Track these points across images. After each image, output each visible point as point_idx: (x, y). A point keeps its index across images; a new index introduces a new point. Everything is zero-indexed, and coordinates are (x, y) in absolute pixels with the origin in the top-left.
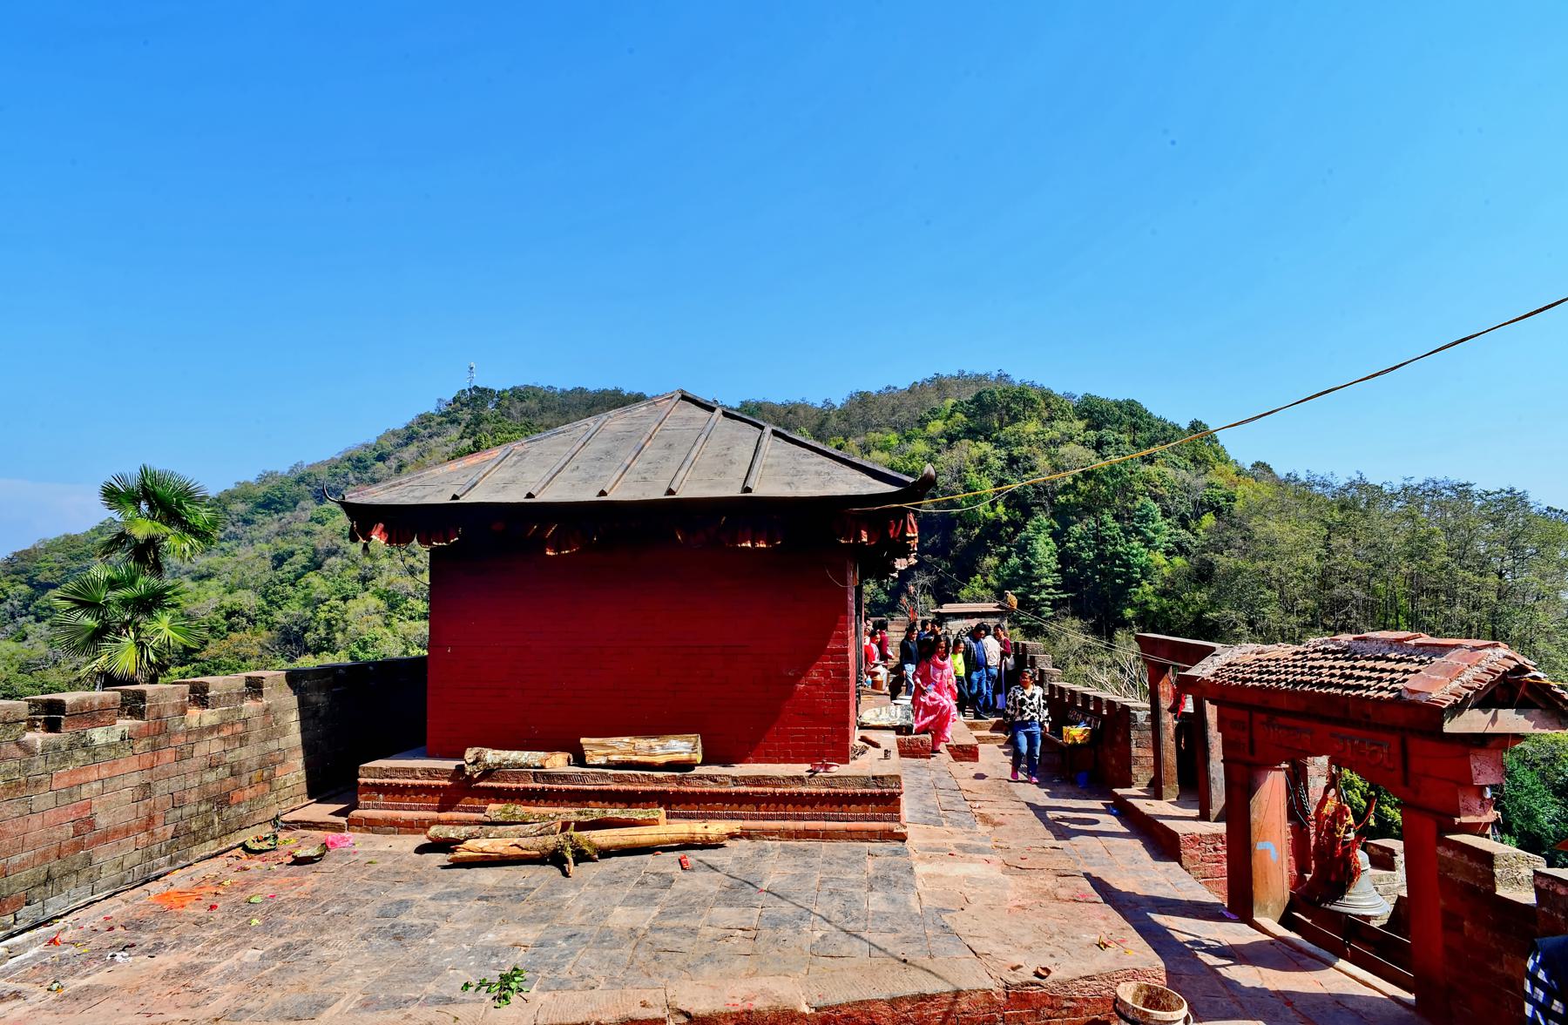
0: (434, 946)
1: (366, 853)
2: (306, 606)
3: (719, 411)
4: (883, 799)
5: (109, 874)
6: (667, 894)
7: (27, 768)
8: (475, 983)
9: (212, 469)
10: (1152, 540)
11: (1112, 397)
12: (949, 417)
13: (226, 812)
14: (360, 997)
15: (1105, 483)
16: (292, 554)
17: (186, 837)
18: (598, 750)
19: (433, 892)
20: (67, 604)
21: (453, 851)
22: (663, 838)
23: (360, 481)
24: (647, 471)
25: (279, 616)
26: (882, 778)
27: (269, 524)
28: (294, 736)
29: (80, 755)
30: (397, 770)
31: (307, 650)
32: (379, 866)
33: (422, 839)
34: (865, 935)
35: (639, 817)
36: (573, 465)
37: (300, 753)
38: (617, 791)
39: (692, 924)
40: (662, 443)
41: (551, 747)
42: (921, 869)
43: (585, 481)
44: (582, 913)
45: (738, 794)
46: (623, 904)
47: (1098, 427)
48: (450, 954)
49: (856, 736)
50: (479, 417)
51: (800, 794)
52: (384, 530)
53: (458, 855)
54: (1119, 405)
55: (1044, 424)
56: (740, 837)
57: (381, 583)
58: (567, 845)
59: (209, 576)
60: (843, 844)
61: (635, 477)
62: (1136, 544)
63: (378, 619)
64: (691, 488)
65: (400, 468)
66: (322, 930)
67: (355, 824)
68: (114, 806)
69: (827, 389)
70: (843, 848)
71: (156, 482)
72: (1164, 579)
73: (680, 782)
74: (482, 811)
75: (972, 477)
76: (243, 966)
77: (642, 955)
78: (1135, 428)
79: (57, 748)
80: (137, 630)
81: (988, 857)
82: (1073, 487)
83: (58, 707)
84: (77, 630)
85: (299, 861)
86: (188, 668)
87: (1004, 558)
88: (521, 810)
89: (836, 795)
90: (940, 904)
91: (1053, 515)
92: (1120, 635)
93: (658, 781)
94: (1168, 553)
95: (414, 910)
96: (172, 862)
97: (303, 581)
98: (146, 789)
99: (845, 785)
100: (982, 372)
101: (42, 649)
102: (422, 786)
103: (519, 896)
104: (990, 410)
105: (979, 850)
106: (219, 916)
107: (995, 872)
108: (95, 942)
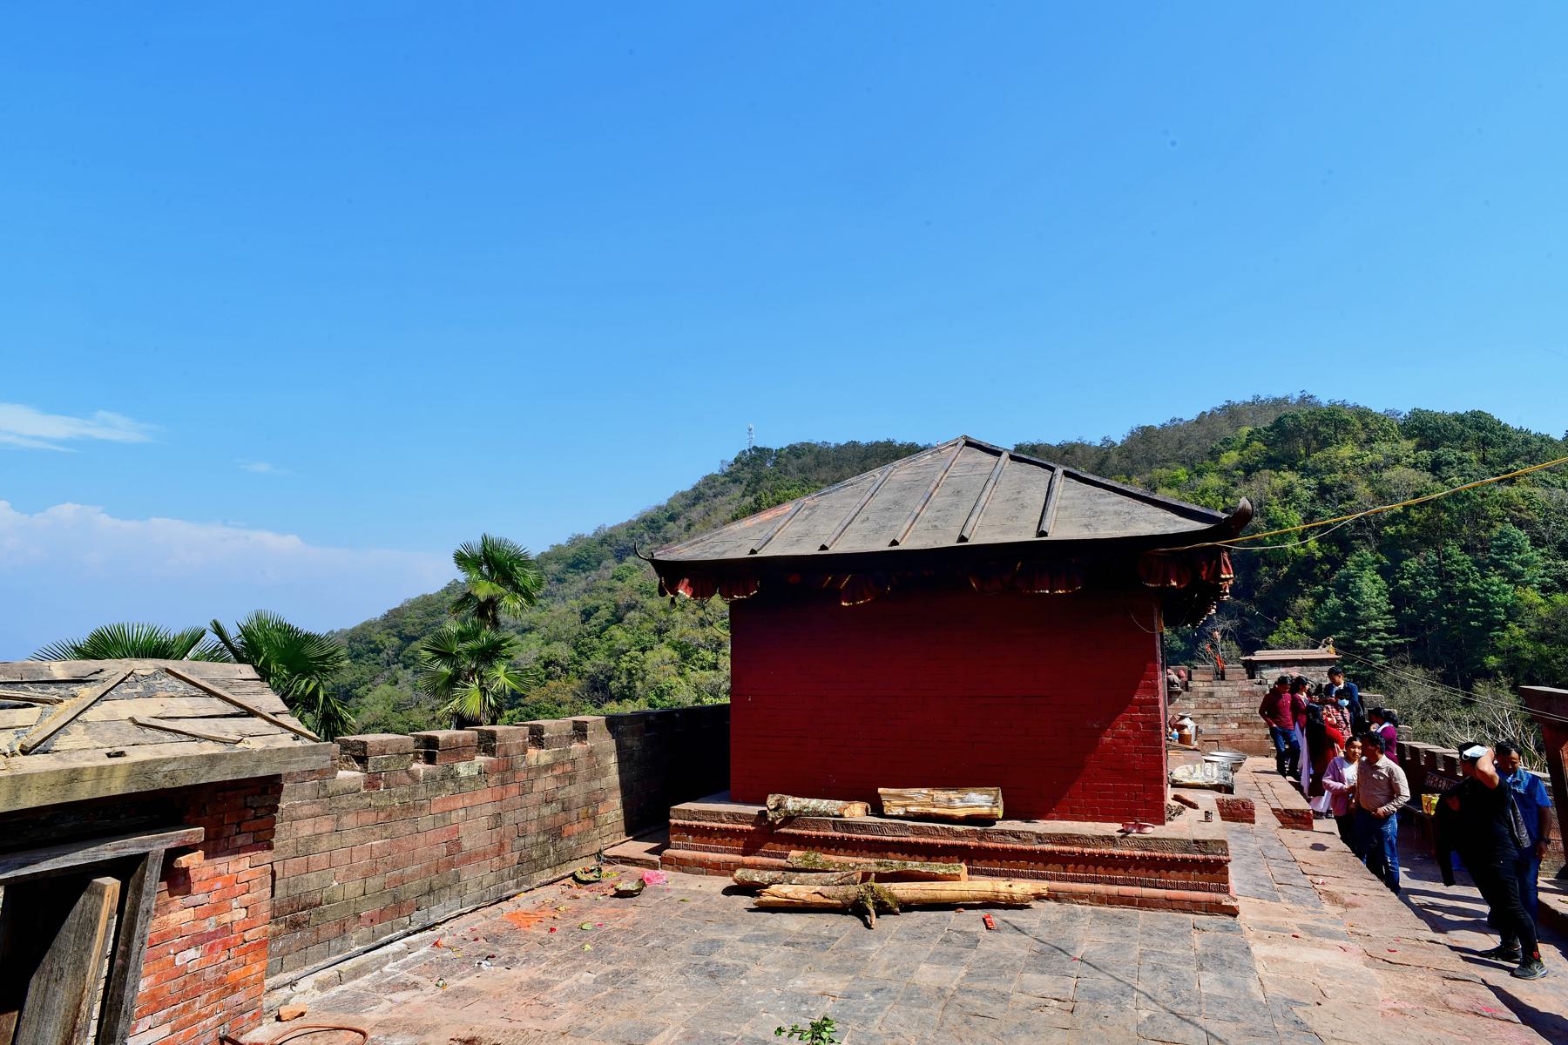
0: (746, 987)
1: (678, 892)
2: (610, 656)
3: (1005, 455)
4: (1207, 867)
5: (473, 892)
6: (972, 956)
7: (414, 794)
8: (788, 1029)
9: (534, 536)
10: (1521, 574)
11: (1449, 410)
12: (1245, 447)
13: (559, 844)
14: (682, 1030)
15: (1446, 510)
16: (597, 609)
17: (528, 865)
18: (904, 801)
19: (739, 929)
20: (429, 655)
21: (759, 895)
22: (966, 894)
23: (654, 540)
24: (937, 518)
25: (587, 666)
26: (1205, 842)
27: (578, 582)
28: (613, 777)
29: (450, 785)
30: (704, 813)
31: (611, 697)
32: (691, 904)
33: (729, 881)
34: (1199, 1020)
35: (940, 871)
36: (863, 516)
37: (618, 793)
38: (917, 844)
39: (1003, 988)
40: (950, 490)
41: (850, 797)
42: (1259, 950)
43: (877, 531)
44: (887, 967)
45: (1043, 852)
46: (928, 961)
47: (1433, 446)
48: (761, 997)
49: (1170, 793)
50: (762, 477)
51: (1111, 856)
52: (690, 585)
53: (763, 899)
54: (1460, 419)
55: (1361, 446)
56: (1046, 898)
57: (674, 634)
58: (869, 896)
59: (530, 630)
60: (1162, 914)
61: (924, 525)
62: (1496, 579)
63: (672, 669)
64: (981, 536)
65: (689, 527)
66: (644, 961)
67: (668, 862)
68: (475, 835)
69: (1106, 425)
70: (1163, 918)
71: (494, 548)
72: (1540, 620)
73: (981, 836)
74: (784, 856)
75: (1277, 511)
76: (581, 986)
77: (953, 1017)
78: (1485, 443)
79: (434, 778)
80: (481, 677)
81: (1343, 943)
82: (1404, 515)
83: (431, 742)
84: (436, 676)
85: (621, 894)
86: (515, 711)
87: (1320, 599)
88: (822, 858)
89: (1153, 858)
90: (1289, 995)
91: (1379, 549)
92: (1481, 688)
93: (958, 835)
94: (1545, 589)
95: (726, 950)
96: (518, 885)
97: (607, 634)
98: (498, 817)
99: (1163, 849)
100: (1280, 395)
101: (408, 692)
102: (727, 829)
103: (823, 944)
104: (1293, 435)
105: (1331, 935)
106: (558, 939)
107: (1355, 963)
108: (465, 948)
